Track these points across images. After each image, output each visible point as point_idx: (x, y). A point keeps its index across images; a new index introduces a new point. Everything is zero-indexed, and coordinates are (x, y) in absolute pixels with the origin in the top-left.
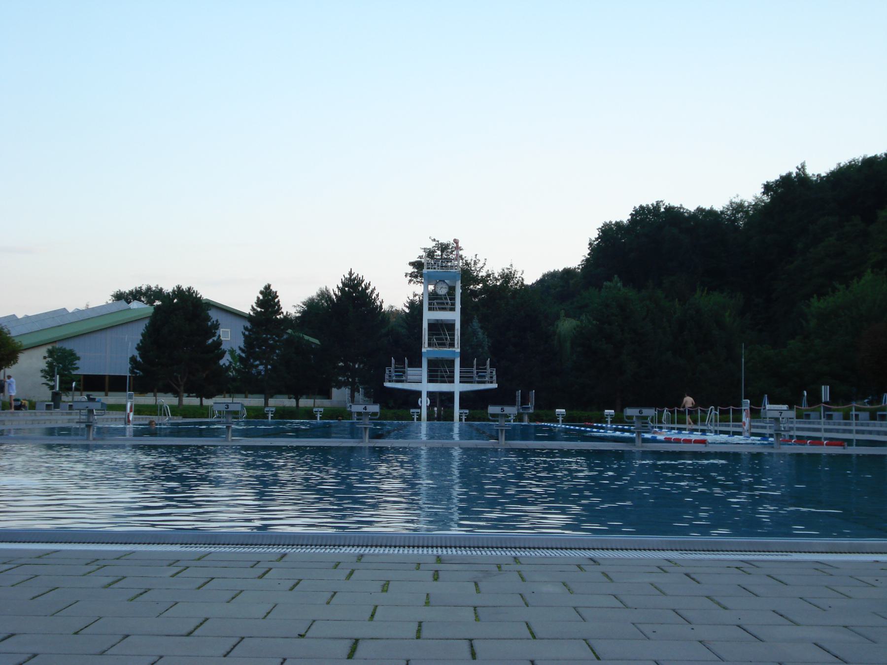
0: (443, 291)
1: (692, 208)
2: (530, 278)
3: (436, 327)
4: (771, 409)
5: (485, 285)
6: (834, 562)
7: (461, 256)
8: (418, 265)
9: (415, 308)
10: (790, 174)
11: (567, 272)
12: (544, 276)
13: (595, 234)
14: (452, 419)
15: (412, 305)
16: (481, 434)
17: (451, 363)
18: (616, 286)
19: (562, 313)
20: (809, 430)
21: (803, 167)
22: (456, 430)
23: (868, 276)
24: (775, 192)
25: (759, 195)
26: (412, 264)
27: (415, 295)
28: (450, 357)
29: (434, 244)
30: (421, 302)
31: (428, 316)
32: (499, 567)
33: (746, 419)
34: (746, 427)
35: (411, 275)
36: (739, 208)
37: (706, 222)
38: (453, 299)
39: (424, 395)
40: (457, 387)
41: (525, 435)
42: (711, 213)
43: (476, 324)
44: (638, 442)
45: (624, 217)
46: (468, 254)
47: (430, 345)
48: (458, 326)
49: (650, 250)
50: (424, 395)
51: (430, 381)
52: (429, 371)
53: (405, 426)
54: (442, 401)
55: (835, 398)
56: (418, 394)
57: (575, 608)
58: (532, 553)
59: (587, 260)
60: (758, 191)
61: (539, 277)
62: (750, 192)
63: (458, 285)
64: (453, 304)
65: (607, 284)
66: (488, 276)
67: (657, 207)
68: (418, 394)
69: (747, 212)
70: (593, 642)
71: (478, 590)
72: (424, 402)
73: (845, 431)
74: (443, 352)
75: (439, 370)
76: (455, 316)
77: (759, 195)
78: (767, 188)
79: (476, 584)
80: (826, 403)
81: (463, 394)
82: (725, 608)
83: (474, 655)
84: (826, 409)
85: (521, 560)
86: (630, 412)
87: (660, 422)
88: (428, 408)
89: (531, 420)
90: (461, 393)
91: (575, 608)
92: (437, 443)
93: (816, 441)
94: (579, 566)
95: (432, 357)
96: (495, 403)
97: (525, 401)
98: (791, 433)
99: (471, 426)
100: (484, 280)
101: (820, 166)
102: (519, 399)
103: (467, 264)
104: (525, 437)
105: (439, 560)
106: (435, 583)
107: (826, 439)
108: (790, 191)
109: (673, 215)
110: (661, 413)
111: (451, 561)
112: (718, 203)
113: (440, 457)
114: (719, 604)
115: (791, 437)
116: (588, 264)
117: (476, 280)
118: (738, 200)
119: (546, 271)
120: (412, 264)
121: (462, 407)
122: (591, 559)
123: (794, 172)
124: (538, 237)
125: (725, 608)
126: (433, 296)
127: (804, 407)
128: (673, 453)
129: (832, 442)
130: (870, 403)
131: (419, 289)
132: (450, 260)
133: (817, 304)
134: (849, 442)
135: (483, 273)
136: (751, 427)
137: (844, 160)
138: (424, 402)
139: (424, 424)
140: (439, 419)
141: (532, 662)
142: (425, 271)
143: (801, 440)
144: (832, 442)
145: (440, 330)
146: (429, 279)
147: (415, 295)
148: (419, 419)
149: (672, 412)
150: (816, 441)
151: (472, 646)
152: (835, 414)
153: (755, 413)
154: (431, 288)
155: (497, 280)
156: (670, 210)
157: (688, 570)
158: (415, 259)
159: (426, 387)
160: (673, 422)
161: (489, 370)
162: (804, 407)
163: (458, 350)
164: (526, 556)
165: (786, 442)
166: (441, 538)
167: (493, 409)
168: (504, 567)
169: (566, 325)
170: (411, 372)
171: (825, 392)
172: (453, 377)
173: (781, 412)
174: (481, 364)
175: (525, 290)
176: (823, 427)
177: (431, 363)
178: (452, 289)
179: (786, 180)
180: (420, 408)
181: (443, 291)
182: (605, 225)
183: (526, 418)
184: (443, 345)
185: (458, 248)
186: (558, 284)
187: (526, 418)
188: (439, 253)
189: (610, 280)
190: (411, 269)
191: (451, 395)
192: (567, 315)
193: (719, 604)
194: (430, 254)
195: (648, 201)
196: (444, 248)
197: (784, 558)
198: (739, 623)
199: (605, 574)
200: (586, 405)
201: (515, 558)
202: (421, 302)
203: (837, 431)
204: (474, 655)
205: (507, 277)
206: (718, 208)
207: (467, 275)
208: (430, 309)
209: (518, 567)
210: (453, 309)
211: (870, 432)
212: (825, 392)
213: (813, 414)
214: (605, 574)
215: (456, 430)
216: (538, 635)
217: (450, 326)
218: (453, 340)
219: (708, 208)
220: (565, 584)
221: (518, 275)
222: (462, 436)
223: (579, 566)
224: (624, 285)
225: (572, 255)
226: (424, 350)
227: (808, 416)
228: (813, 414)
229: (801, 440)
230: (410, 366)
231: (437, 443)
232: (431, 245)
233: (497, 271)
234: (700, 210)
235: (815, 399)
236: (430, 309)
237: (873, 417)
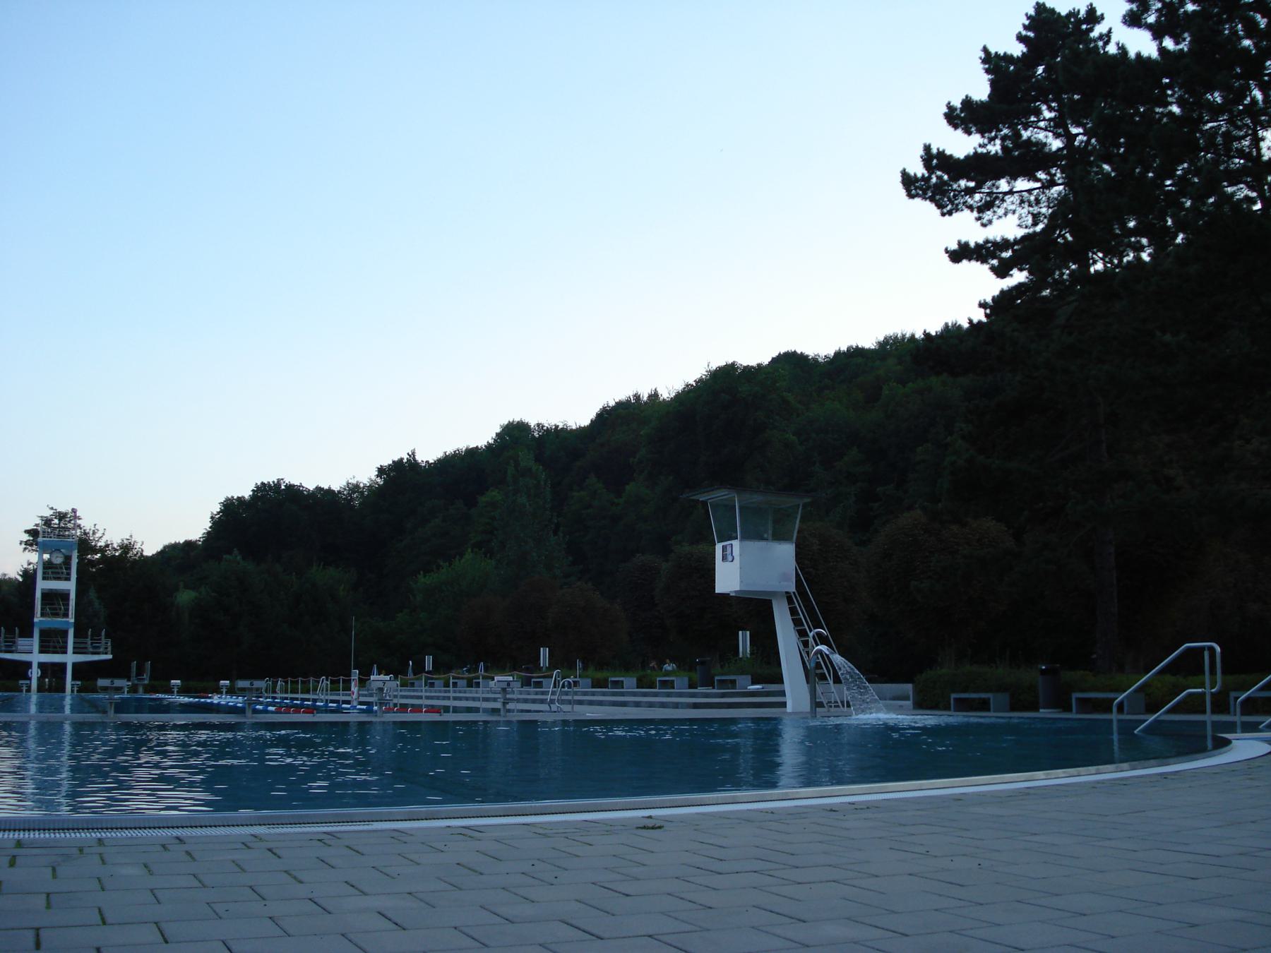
0: (58, 560)
1: (311, 487)
2: (150, 549)
3: (49, 596)
4: (376, 678)
5: (103, 556)
6: (412, 829)
7: (79, 526)
8: (33, 533)
9: (29, 576)
10: (402, 459)
11: (189, 544)
12: (165, 547)
13: (217, 508)
14: (63, 690)
15: (26, 574)
16: (95, 707)
17: (65, 633)
18: (235, 559)
19: (182, 584)
20: (412, 697)
21: (413, 453)
22: (68, 701)
23: (468, 555)
24: (388, 475)
25: (373, 478)
26: (27, 532)
27: (29, 564)
28: (64, 627)
29: (51, 512)
30: (35, 571)
31: (42, 585)
32: (81, 850)
33: (354, 688)
34: (355, 696)
35: (26, 543)
36: (355, 488)
37: (324, 498)
38: (69, 568)
39: (35, 666)
40: (70, 658)
41: (140, 707)
42: (330, 492)
43: (92, 594)
44: (249, 713)
45: (246, 493)
46: (86, 523)
47: (42, 615)
48: (73, 596)
49: (268, 523)
50: (35, 666)
51: (41, 652)
52: (41, 641)
53: (13, 697)
54: (53, 673)
55: (437, 667)
56: (28, 665)
57: (152, 890)
58: (199, 832)
59: (208, 533)
60: (373, 474)
61: (159, 548)
62: (366, 475)
63: (75, 555)
64: (69, 574)
65: (226, 557)
66: (107, 546)
67: (278, 485)
68: (28, 665)
69: (362, 493)
70: (163, 925)
71: (54, 875)
72: (35, 673)
73: (444, 698)
74: (57, 622)
75: (52, 641)
76: (70, 586)
77: (373, 478)
78: (381, 471)
79: (54, 870)
80: (429, 672)
81: (75, 665)
82: (301, 882)
83: (38, 945)
84: (427, 679)
85: (106, 842)
86: (242, 684)
87: (274, 692)
88: (39, 679)
89: (146, 691)
90: (75, 665)
91: (152, 890)
92: (46, 716)
93: (417, 709)
94: (163, 846)
95: (46, 626)
96: (103, 677)
97: (140, 672)
98: (395, 701)
99: (83, 699)
100: (102, 550)
101: (428, 454)
102: (134, 669)
103: (85, 533)
104: (138, 710)
105: (19, 844)
106: (12, 869)
107: (426, 706)
108: (402, 475)
109: (294, 492)
110: (275, 684)
111: (33, 845)
112: (336, 483)
113: (49, 731)
114: (295, 878)
115: (395, 705)
116: (209, 536)
117: (94, 550)
118: (354, 481)
119: (167, 543)
120: (27, 532)
121: (74, 678)
122: (178, 838)
123: (405, 457)
124: (159, 508)
125: (301, 882)
126: (48, 566)
127: (410, 675)
128: (273, 723)
129: (432, 709)
130: (468, 671)
131: (34, 557)
132: (68, 529)
133: (423, 580)
134: (446, 709)
135: (102, 543)
136: (359, 695)
137: (450, 450)
138: (35, 673)
139: (34, 697)
140: (50, 690)
141: (98, 950)
142: (40, 539)
143: (403, 708)
144: (432, 709)
145: (54, 600)
146: (43, 548)
147: (29, 564)
148: (29, 690)
149: (286, 682)
150: (417, 709)
151: (38, 935)
152: (437, 682)
153: (363, 682)
154: (46, 556)
155: (116, 550)
156: (290, 487)
157: (270, 845)
158: (31, 527)
159: (37, 658)
160: (286, 692)
161: (103, 641)
162: (410, 675)
163: (72, 621)
164: (112, 838)
165: (389, 710)
166: (77, 820)
167: (102, 682)
168: (86, 850)
169: (185, 597)
170: (22, 642)
171: (429, 662)
172: (66, 647)
173: (384, 682)
174: (96, 634)
175: (145, 561)
176: (424, 694)
177: (43, 633)
178: (68, 559)
179: (398, 465)
180: (30, 679)
181: (58, 560)
182: (227, 499)
183: (141, 689)
184: (56, 615)
185: (76, 517)
186: (178, 555)
187: (141, 689)
188: (56, 521)
189: (230, 553)
190: (26, 537)
191: (1213, 712)
192: (187, 587)
193: (295, 878)
194: (47, 522)
195: (270, 478)
196: (62, 516)
197: (366, 828)
198: (310, 896)
199: (188, 853)
200: (201, 678)
201: (100, 839)
202: (35, 571)
203: (438, 698)
204: (38, 945)
205: (126, 548)
206: (336, 488)
207: (85, 545)
208: (44, 578)
209: (101, 849)
210: (68, 579)
211: (467, 699)
212: (429, 662)
213: (416, 683)
214: (188, 853)
215: (68, 701)
216: (109, 920)
217: (64, 596)
218: (67, 610)
219: (326, 487)
220: (146, 866)
221: (138, 546)
222: (72, 710)
223: (163, 846)
224: (244, 559)
225: (195, 527)
226: (36, 620)
227: (412, 685)
228: (416, 683)
229: (403, 708)
230: (21, 636)
231: (46, 716)
232: (48, 513)
233: (116, 542)
234: (319, 489)
235: (419, 669)
236: (44, 578)
237: (470, 685)
